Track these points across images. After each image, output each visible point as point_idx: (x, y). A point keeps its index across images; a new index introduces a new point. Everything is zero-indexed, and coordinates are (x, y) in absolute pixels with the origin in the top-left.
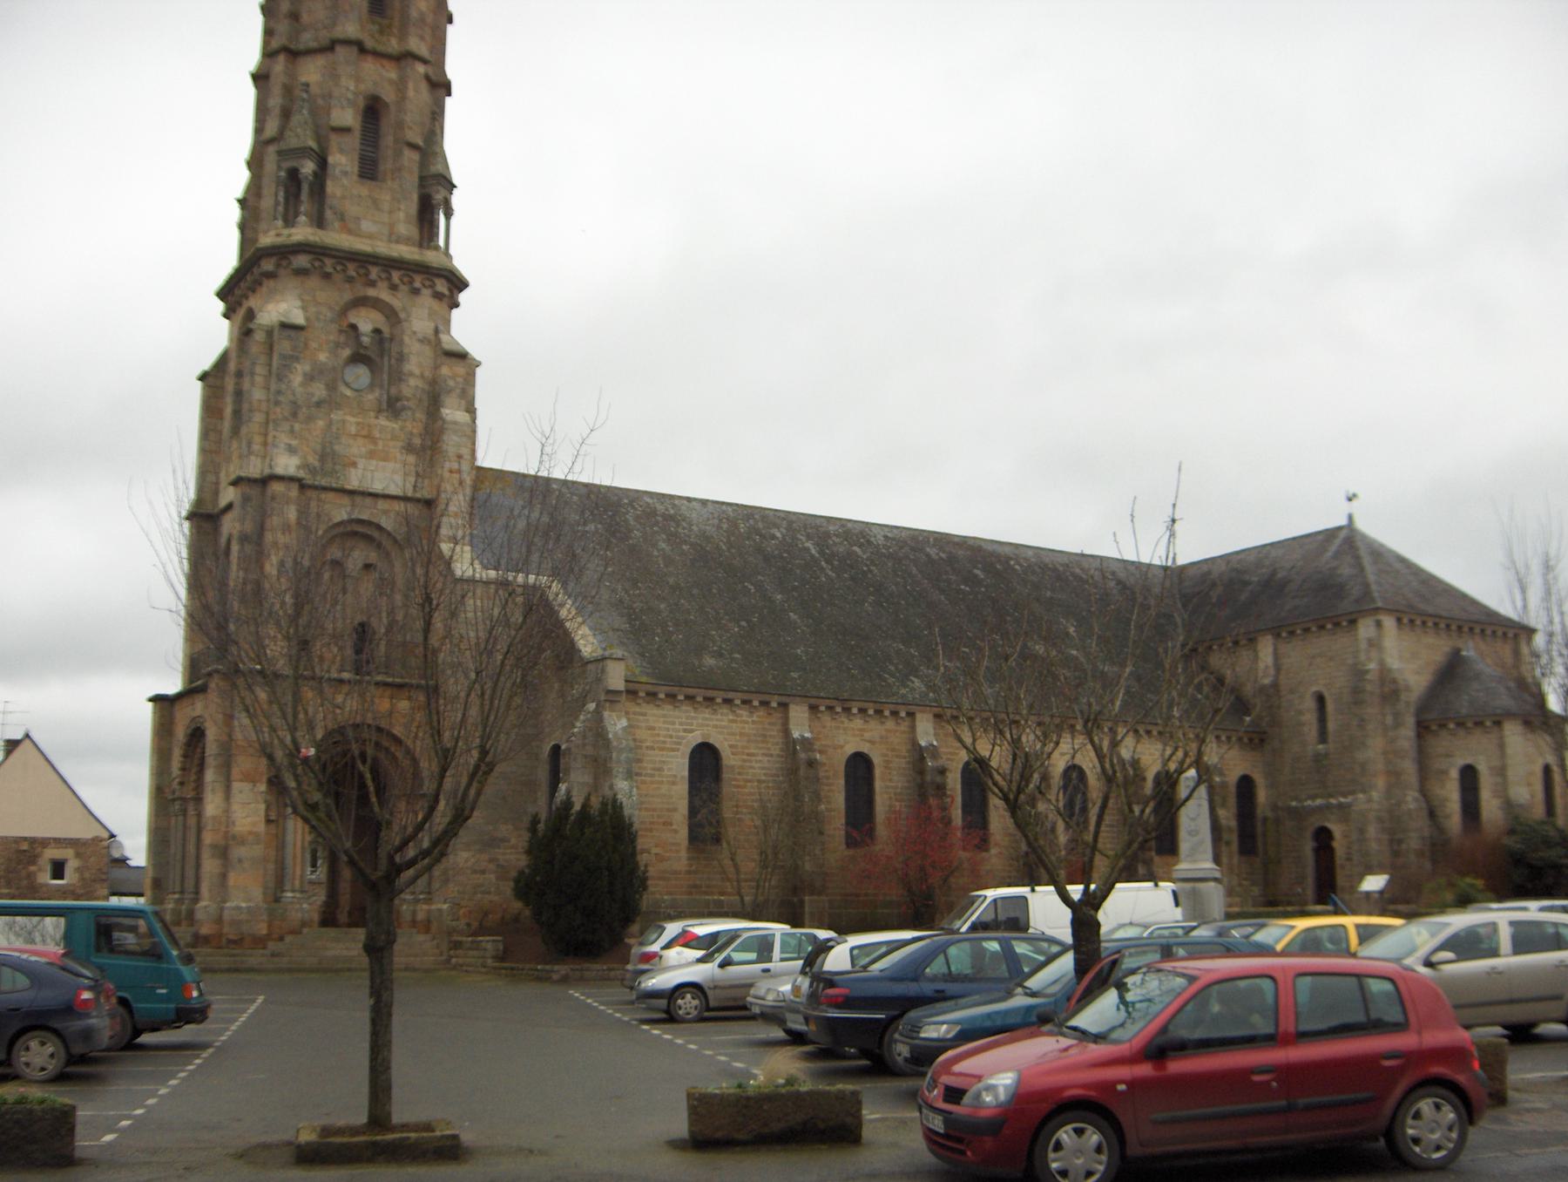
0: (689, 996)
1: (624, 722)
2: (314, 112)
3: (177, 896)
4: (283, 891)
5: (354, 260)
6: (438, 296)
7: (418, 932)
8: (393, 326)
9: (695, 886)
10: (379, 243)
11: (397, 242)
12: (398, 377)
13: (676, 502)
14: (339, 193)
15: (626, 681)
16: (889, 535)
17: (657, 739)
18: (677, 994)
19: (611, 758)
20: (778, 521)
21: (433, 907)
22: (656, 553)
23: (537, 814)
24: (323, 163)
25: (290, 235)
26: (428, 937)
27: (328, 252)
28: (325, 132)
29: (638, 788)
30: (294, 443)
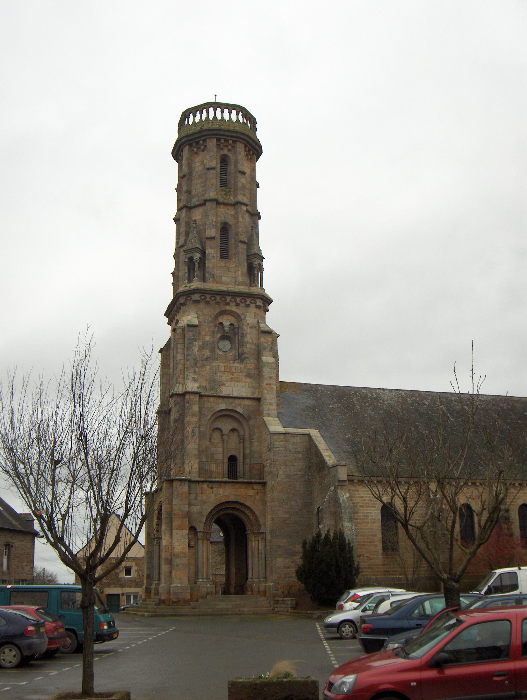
0: (347, 626)
1: (348, 495)
2: (198, 232)
3: (156, 582)
4: (198, 579)
5: (218, 294)
6: (258, 307)
7: (261, 597)
8: (239, 322)
9: (387, 571)
10: (230, 286)
11: (238, 285)
12: (242, 344)
13: (378, 391)
14: (211, 266)
15: (347, 476)
16: (482, 399)
17: (365, 502)
18: (341, 626)
19: (342, 512)
20: (426, 396)
21: (267, 584)
22: (366, 415)
23: (305, 540)
24: (203, 253)
25: (190, 286)
26: (265, 598)
27: (207, 292)
28: (203, 240)
29: (356, 525)
30: (196, 377)
